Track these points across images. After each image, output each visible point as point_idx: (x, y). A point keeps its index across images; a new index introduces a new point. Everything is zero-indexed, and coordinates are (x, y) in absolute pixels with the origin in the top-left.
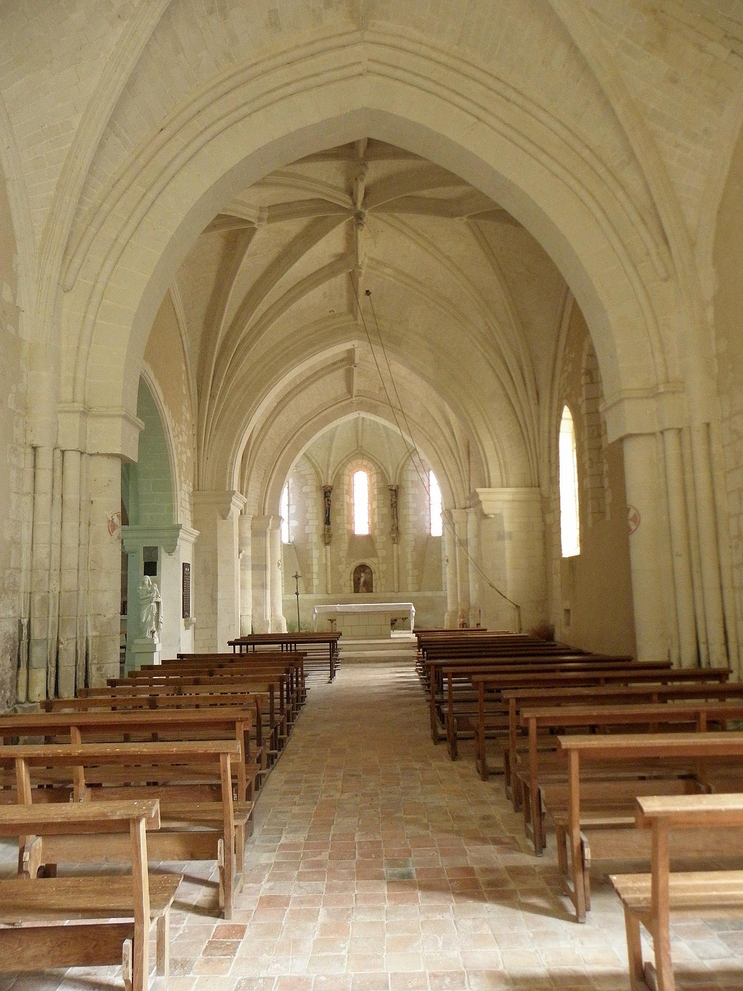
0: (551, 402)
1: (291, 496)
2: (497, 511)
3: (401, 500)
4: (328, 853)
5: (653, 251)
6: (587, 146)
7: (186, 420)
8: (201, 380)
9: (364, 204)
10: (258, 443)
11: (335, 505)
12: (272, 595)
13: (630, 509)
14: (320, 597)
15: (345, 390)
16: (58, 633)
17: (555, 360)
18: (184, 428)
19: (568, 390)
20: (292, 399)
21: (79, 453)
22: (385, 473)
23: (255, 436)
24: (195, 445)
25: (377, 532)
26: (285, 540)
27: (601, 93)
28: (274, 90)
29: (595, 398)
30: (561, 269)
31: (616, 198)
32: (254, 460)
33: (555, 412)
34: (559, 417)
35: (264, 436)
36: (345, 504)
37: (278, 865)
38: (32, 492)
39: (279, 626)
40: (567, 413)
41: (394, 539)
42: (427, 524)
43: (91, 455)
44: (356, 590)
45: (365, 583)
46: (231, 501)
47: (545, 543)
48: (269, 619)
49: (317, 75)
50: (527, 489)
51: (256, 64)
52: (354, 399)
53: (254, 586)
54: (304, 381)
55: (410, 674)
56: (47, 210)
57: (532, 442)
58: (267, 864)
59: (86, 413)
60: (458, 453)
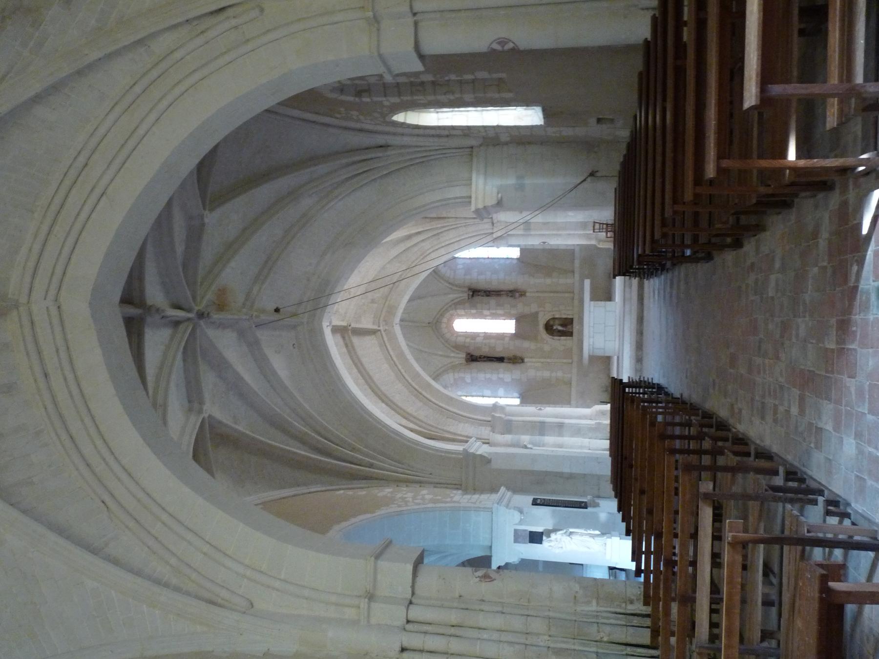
0: (388, 133)
1: (474, 394)
2: (495, 190)
3: (483, 286)
4: (848, 379)
5: (234, 22)
6: (131, 87)
7: (391, 493)
8: (354, 477)
9: (189, 310)
10: (420, 423)
11: (485, 351)
12: (571, 417)
13: (492, 48)
14: (575, 371)
15: (373, 336)
16: (591, 641)
17: (346, 128)
18: (399, 495)
19: (376, 115)
20: (379, 389)
21: (411, 607)
22: (456, 301)
23: (412, 426)
24: (418, 486)
25: (513, 312)
26: (517, 401)
27: (80, 73)
28: (70, 392)
29: (386, 89)
30: (249, 116)
31: (182, 59)
32: (436, 428)
33: (399, 130)
34: (403, 125)
35: (415, 418)
36: (484, 341)
37: (858, 435)
38: (446, 656)
39: (603, 413)
40: (400, 118)
41: (521, 295)
42: (508, 262)
43: (413, 594)
44: (570, 334)
45: (562, 325)
46: (473, 453)
47: (529, 143)
48: (593, 422)
49: (57, 351)
50: (475, 159)
51: (46, 408)
52: (381, 328)
53: (560, 435)
54: (363, 376)
55: (653, 285)
56: (173, 618)
57: (428, 154)
58: (857, 447)
59: (371, 597)
60: (437, 228)
